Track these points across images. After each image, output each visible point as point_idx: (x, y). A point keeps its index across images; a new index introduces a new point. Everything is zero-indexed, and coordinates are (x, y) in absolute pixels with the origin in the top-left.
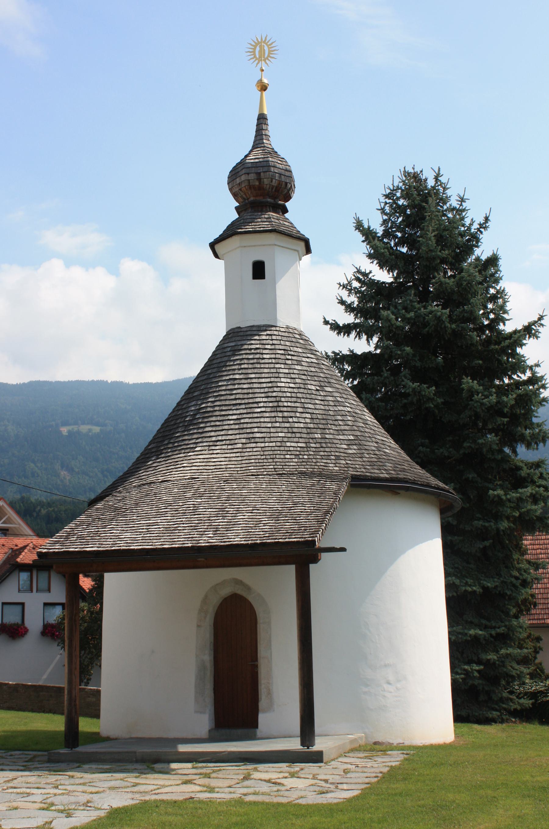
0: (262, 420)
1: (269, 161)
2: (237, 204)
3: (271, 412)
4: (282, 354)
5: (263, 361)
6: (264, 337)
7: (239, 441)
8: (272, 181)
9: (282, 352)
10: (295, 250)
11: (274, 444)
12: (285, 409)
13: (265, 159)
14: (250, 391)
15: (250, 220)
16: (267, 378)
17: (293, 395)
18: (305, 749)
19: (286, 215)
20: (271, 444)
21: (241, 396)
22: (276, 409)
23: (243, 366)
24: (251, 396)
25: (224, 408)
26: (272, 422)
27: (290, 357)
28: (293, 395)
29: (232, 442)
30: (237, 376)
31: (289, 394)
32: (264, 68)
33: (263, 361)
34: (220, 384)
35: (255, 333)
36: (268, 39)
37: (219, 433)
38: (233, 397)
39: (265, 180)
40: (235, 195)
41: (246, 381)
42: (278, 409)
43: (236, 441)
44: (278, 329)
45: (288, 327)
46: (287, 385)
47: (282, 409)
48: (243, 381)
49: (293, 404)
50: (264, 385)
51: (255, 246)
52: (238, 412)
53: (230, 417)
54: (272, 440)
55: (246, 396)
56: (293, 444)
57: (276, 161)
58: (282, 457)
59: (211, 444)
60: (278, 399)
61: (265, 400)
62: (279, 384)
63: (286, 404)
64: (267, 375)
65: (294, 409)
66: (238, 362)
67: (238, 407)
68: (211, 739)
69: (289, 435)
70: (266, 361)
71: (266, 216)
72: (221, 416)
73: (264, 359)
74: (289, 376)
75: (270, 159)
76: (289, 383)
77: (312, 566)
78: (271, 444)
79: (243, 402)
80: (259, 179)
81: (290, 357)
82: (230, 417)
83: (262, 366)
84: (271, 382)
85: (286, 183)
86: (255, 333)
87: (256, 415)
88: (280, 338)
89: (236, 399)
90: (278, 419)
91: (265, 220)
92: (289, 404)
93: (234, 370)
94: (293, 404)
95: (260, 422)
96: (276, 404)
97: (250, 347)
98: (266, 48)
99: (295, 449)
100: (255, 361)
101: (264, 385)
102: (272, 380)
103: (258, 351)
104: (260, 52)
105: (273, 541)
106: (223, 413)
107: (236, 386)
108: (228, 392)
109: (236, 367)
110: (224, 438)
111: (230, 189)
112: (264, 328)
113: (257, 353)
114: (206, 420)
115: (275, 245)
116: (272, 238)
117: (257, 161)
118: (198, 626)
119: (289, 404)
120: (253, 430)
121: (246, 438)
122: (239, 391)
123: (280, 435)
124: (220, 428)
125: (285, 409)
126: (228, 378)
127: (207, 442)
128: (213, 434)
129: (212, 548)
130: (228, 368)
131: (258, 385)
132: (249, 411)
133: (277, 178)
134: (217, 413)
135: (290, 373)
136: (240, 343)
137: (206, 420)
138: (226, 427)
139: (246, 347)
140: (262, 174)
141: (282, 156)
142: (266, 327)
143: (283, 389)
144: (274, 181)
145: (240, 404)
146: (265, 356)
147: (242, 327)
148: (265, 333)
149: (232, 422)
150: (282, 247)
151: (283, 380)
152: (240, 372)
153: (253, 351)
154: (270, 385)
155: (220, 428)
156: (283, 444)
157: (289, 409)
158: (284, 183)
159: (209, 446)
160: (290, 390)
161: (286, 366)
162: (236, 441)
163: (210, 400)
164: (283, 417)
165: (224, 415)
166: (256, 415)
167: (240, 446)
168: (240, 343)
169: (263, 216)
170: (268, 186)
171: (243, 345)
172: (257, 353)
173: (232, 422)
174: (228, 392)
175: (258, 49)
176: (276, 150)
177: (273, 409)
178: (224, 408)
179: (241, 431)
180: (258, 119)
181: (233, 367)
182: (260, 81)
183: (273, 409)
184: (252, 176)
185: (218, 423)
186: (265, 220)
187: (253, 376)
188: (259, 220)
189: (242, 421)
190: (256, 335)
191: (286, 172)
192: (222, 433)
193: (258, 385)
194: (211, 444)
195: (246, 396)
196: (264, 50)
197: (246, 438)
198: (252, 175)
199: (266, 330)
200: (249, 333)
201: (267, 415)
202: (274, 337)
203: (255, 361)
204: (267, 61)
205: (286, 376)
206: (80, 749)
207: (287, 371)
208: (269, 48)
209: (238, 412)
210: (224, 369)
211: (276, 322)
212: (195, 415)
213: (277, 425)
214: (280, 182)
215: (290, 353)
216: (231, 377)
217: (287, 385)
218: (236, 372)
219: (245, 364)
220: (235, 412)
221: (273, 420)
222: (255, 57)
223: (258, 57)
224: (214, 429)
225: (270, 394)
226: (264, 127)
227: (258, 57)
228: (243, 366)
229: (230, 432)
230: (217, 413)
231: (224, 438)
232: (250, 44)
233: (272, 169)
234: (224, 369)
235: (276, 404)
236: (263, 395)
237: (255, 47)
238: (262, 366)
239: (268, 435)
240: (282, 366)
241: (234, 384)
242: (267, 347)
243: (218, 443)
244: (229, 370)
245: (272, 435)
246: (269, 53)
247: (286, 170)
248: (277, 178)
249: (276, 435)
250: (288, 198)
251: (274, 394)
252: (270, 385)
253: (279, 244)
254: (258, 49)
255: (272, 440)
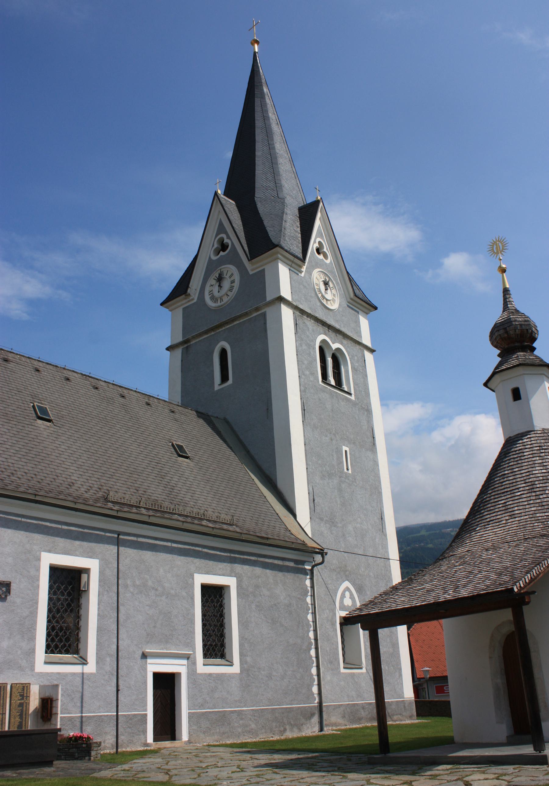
0: (521, 500)
1: (510, 318)
2: (499, 352)
3: (527, 493)
4: (538, 450)
5: (524, 458)
6: (525, 441)
7: (504, 519)
8: (515, 331)
9: (538, 448)
10: (541, 374)
11: (527, 517)
12: (538, 489)
13: (508, 318)
14: (514, 481)
15: (505, 362)
16: (526, 469)
17: (544, 478)
18: (537, 753)
19: (535, 353)
20: (525, 517)
21: (508, 486)
22: (531, 490)
23: (510, 464)
24: (514, 484)
25: (496, 497)
26: (528, 501)
27: (543, 451)
28: (544, 478)
29: (500, 520)
30: (506, 472)
31: (541, 478)
32: (501, 258)
33: (524, 458)
34: (496, 480)
35: (519, 439)
36: (500, 238)
37: (492, 515)
38: (503, 487)
39: (511, 331)
40: (496, 347)
41: (512, 474)
42: (533, 490)
43: (502, 519)
44: (535, 432)
45: (543, 430)
46: (540, 471)
47: (535, 490)
48: (510, 475)
49: (544, 485)
50: (524, 475)
51: (511, 378)
52: (505, 497)
53: (500, 502)
54: (527, 513)
55: (511, 485)
56: (541, 515)
57: (516, 317)
58: (532, 525)
59: (486, 524)
60: (533, 483)
61: (524, 485)
62: (534, 472)
63: (538, 486)
64: (526, 467)
65: (545, 488)
66: (508, 462)
67: (505, 494)
68: (510, 742)
69: (540, 508)
70: (526, 457)
71: (515, 356)
72: (494, 502)
73: (524, 456)
74: (542, 465)
75: (512, 317)
76: (542, 470)
77: (525, 608)
78: (525, 517)
79: (509, 489)
80: (507, 332)
81: (543, 451)
82: (500, 502)
83: (523, 461)
84: (528, 472)
85: (527, 330)
86: (519, 439)
87: (517, 498)
88: (537, 438)
89: (504, 489)
90: (532, 498)
91: (515, 359)
92: (541, 485)
93: (505, 468)
94: (544, 485)
95: (520, 502)
96: (531, 487)
97: (516, 449)
98: (500, 245)
99: (543, 518)
100: (519, 458)
101: (524, 475)
102: (530, 469)
103: (521, 451)
104: (497, 248)
105: (485, 592)
106: (496, 500)
107: (505, 479)
108: (500, 485)
109: (506, 466)
110: (495, 518)
111: (492, 344)
112: (526, 434)
113: (520, 453)
114: (485, 507)
115: (524, 374)
116: (520, 370)
117: (503, 320)
118: (490, 658)
119: (541, 485)
120: (513, 509)
121: (509, 516)
122: (507, 482)
123: (533, 509)
124: (492, 512)
125: (538, 489)
126: (500, 474)
127: (484, 523)
128: (488, 516)
129: (447, 602)
130: (501, 467)
131: (520, 476)
132: (512, 495)
133: (519, 328)
134: (492, 501)
135: (543, 463)
136: (509, 448)
137: (485, 507)
138: (497, 510)
139: (513, 450)
140: (508, 328)
141: (523, 312)
142: (528, 433)
143: (537, 475)
144: (517, 330)
145: (507, 492)
146: (525, 454)
147: (511, 436)
148: (526, 437)
149: (501, 506)
150: (530, 374)
151: (537, 468)
152: (508, 468)
153: (517, 452)
154: (528, 474)
155: (492, 512)
156: (534, 515)
157: (541, 489)
158: (525, 330)
159: (485, 525)
160: (542, 475)
161: (540, 458)
162: (502, 519)
163: (489, 492)
164: (536, 496)
165: (496, 502)
166: (517, 498)
167: (504, 522)
168: (509, 448)
169: (514, 356)
170: (514, 335)
171: (511, 449)
172: (520, 453)
173: (501, 506)
174: (500, 485)
175: (495, 246)
176: (518, 309)
177: (529, 491)
178: (496, 497)
179: (506, 511)
180: (503, 292)
181: (505, 466)
182: (500, 267)
183: (529, 491)
184: (502, 332)
185: (492, 508)
186: (515, 359)
187: (517, 469)
188: (511, 360)
189: (507, 504)
190: (519, 440)
191: (526, 322)
192: (494, 515)
193: (520, 476)
194: (486, 524)
195: (511, 485)
196: (499, 246)
197: (509, 516)
198: (501, 330)
199: (527, 435)
200: (515, 440)
201: (525, 496)
202: (532, 439)
203: (519, 458)
204: (502, 252)
205: (540, 465)
206: (390, 755)
207: (540, 461)
208: (502, 244)
209: (505, 497)
210: (499, 469)
211: (534, 428)
212: (480, 505)
213: (532, 502)
214: (522, 330)
215: (544, 448)
216: (503, 473)
217: (540, 471)
218: (506, 469)
219: (512, 462)
220: (503, 498)
221: (529, 499)
222: (494, 252)
223: (496, 252)
224: (489, 513)
225: (527, 481)
226: (508, 296)
227: (496, 252)
228: (510, 464)
229: (499, 513)
230: (492, 501)
231: (495, 518)
232: (490, 245)
233: (514, 323)
234: (499, 469)
235: (531, 487)
236: (523, 482)
237: (493, 246)
238: (523, 461)
239: (524, 511)
240: (538, 458)
241: (504, 478)
242: (527, 447)
243: (491, 523)
244: (502, 469)
245: (527, 510)
246: (493, 247)
247: (525, 321)
248: (519, 328)
249: (530, 509)
250: (534, 339)
251: (531, 480)
252: (528, 474)
253: (527, 373)
254: (495, 246)
255: (527, 513)
